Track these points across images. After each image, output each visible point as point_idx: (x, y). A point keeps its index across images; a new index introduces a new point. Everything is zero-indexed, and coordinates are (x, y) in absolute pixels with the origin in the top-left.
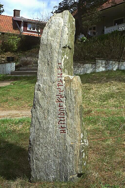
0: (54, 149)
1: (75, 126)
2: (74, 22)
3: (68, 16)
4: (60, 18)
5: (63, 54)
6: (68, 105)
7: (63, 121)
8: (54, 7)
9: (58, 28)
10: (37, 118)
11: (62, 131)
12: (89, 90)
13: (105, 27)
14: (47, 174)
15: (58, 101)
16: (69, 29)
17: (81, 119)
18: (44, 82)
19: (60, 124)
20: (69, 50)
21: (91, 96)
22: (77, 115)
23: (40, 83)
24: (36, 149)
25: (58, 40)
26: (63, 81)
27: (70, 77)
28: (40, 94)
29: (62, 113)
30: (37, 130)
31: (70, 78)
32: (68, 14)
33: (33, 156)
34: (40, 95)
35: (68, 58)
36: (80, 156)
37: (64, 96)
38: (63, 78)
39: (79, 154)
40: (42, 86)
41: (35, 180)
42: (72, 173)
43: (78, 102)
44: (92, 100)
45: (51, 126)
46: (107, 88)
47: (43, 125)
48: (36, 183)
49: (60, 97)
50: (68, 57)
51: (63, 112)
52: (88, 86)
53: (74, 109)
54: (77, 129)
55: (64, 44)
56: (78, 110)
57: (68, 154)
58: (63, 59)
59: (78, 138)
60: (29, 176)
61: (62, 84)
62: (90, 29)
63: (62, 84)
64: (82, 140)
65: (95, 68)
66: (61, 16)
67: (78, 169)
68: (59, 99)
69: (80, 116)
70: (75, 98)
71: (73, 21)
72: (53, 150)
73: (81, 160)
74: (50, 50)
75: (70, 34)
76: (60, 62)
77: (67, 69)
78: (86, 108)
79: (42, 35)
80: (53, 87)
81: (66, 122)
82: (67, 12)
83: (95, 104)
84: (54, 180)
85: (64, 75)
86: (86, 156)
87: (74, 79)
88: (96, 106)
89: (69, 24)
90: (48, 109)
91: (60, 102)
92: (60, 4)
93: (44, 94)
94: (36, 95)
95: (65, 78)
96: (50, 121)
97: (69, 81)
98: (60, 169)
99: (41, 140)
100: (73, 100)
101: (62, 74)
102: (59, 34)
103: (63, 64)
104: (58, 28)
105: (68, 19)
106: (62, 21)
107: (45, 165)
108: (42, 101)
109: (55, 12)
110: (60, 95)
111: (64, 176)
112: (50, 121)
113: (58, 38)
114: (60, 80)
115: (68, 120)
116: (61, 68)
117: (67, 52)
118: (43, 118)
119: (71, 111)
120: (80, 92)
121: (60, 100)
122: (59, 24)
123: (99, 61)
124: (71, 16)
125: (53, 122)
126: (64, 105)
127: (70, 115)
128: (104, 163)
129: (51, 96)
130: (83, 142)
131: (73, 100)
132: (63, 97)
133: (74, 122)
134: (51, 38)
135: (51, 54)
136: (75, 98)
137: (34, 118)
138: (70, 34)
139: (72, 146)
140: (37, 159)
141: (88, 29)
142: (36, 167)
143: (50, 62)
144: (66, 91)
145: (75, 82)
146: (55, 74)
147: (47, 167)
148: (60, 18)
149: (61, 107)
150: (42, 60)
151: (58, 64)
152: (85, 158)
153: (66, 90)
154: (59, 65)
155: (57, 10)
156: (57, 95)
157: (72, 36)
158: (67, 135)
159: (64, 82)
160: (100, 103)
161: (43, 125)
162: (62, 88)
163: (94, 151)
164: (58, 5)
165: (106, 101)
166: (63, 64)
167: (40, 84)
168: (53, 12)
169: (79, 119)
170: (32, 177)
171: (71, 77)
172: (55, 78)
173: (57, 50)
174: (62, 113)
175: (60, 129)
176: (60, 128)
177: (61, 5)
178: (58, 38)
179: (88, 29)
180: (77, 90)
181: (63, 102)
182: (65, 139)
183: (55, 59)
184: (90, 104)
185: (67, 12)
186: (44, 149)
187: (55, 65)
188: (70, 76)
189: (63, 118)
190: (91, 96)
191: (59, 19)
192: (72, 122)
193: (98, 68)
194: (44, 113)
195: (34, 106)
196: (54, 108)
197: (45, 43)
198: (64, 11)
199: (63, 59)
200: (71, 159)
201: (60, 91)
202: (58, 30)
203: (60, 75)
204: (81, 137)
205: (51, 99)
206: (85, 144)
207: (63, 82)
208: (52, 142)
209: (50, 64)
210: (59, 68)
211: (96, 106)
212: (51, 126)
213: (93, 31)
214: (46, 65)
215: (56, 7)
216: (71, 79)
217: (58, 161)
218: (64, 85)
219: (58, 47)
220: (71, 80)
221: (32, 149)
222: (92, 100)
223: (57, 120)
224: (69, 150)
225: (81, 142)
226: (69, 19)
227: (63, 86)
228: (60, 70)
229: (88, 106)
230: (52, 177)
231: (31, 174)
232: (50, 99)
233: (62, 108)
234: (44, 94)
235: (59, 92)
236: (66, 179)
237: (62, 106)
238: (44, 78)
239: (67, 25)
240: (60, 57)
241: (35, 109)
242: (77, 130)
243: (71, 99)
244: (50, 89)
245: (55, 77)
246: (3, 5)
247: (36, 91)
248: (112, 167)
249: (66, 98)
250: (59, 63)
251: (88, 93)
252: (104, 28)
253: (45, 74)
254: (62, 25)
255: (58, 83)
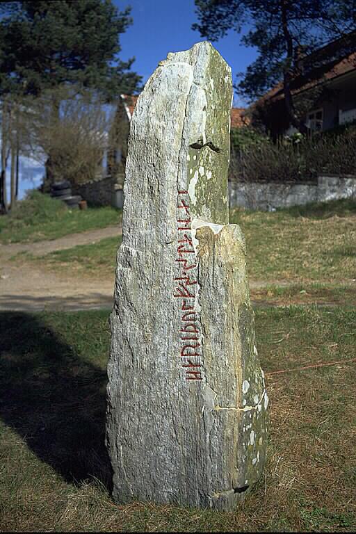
0: (171, 421)
1: (227, 361)
2: (227, 77)
3: (208, 59)
4: (186, 65)
5: (194, 165)
6: (206, 305)
7: (194, 347)
8: (237, 76)
9: (176, 93)
10: (125, 339)
11: (192, 373)
12: (300, 239)
13: (340, 111)
14: (155, 485)
15: (179, 293)
16: (211, 95)
17: (242, 342)
18: (142, 243)
19: (185, 355)
20: (212, 156)
21: (303, 253)
22: (233, 332)
23: (129, 246)
24: (124, 417)
25: (177, 127)
26: (193, 238)
27: (211, 228)
28: (130, 275)
29: (191, 326)
30: (126, 370)
31: (213, 230)
32: (209, 51)
33: (117, 436)
34: (130, 277)
35: (209, 175)
36: (240, 442)
37: (195, 279)
38: (193, 232)
39: (237, 437)
40: (134, 254)
41: (123, 497)
42: (218, 487)
43: (236, 297)
44: (305, 262)
45: (162, 360)
46: (338, 236)
47: (142, 358)
48: (124, 505)
49: (184, 284)
50: (208, 170)
51: (192, 322)
52: (298, 232)
53: (223, 315)
54: (231, 370)
55: (195, 134)
56: (237, 319)
57: (208, 435)
58: (194, 180)
59: (236, 393)
60: (110, 486)
61: (190, 247)
62: (311, 117)
63: (190, 247)
64: (248, 399)
65: (317, 194)
66: (188, 58)
67: (236, 475)
68: (182, 288)
69: (239, 335)
70: (226, 286)
71: (226, 74)
72: (168, 422)
73: (244, 453)
74: (155, 156)
75: (213, 108)
76: (183, 186)
77: (207, 206)
78: (293, 279)
79: (134, 113)
80: (167, 257)
81: (201, 351)
82: (203, 46)
83: (313, 269)
84: (174, 501)
85: (197, 223)
86: (261, 439)
87: (224, 234)
88: (314, 275)
89: (212, 81)
90: (152, 314)
91: (186, 296)
92: (249, 69)
93: (140, 275)
94: (119, 277)
95: (198, 231)
96: (159, 347)
97: (208, 239)
98: (188, 473)
99: (136, 396)
100: (222, 291)
101: (189, 220)
102: (179, 109)
103: (192, 192)
104: (176, 93)
105: (207, 65)
106: (188, 72)
107: (149, 459)
108: (136, 294)
109: (239, 85)
110: (186, 278)
111: (199, 492)
112: (159, 347)
113: (177, 120)
114: (185, 236)
115: (207, 346)
116: (186, 204)
117: (207, 160)
118: (142, 340)
119: (214, 322)
120: (241, 270)
121: (186, 292)
122: (181, 80)
123: (324, 178)
124: (217, 60)
125: (166, 349)
126: (196, 303)
127: (212, 330)
128: (316, 438)
129: (161, 281)
130: (250, 403)
131: (222, 291)
132: (192, 282)
133: (227, 352)
134: (158, 122)
135: (158, 167)
136: (226, 286)
137: (117, 338)
138: (213, 108)
139: (216, 414)
140: (127, 443)
141: (308, 117)
142: (126, 463)
143: (156, 189)
144: (202, 266)
145: (226, 242)
146: (169, 221)
147: (153, 465)
148: (183, 64)
149: (188, 309)
150: (134, 183)
151: (179, 193)
152: (258, 443)
153: (200, 266)
154: (181, 195)
155: (243, 80)
156: (176, 279)
157: (221, 115)
158: (205, 385)
159: (195, 242)
160: (323, 268)
161: (142, 358)
162: (191, 259)
163: (293, 400)
164: (245, 71)
165: (336, 264)
166: (192, 192)
167: (130, 249)
168: (237, 86)
169: (239, 344)
170: (117, 488)
171: (216, 228)
172: (170, 231)
173: (173, 154)
174: (192, 325)
175: (186, 369)
176: (186, 367)
177: (251, 71)
178: (177, 120)
179: (308, 117)
180: (231, 265)
181: (194, 297)
182: (199, 397)
183: (169, 177)
184: (300, 272)
185: (203, 46)
186: (146, 418)
187: (170, 196)
188: (212, 226)
189: (193, 339)
190: (303, 253)
191: (182, 67)
192: (219, 349)
193: (322, 193)
194: (142, 325)
195: (116, 307)
196: (169, 313)
197: (142, 136)
198: (198, 45)
199: (194, 180)
200: (216, 449)
201: (185, 265)
202: (178, 98)
203: (184, 223)
204: (245, 392)
205: (162, 289)
206: (256, 408)
207: (193, 242)
208: (166, 402)
209: (157, 193)
210: (182, 205)
211: (314, 275)
212: (162, 360)
213: (315, 120)
214: (146, 196)
215: (242, 74)
216: (215, 233)
217: (184, 450)
218: (195, 250)
219: (176, 145)
220: (215, 236)
221: (115, 419)
222: (305, 262)
223: (178, 345)
224: (209, 427)
225: (244, 404)
226: (210, 66)
227: (194, 252)
228: (183, 211)
229: (296, 275)
230: (167, 492)
231: (114, 479)
232: (157, 288)
233: (190, 313)
234: (140, 275)
235: (182, 270)
236: (204, 501)
237: (191, 308)
238: (141, 232)
239: (201, 81)
240: (183, 174)
241: (117, 314)
242: (233, 373)
243: (216, 290)
244: (158, 262)
245: (171, 228)
246: (141, 77)
247: (120, 267)
248: (337, 450)
249: (201, 286)
250: (181, 189)
251: (297, 247)
252: (338, 114)
253: (143, 222)
254: (190, 83)
255: (179, 244)
